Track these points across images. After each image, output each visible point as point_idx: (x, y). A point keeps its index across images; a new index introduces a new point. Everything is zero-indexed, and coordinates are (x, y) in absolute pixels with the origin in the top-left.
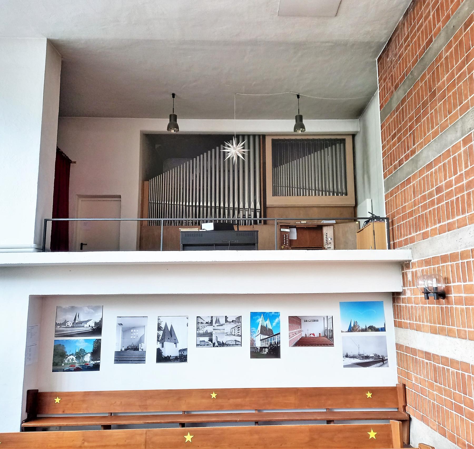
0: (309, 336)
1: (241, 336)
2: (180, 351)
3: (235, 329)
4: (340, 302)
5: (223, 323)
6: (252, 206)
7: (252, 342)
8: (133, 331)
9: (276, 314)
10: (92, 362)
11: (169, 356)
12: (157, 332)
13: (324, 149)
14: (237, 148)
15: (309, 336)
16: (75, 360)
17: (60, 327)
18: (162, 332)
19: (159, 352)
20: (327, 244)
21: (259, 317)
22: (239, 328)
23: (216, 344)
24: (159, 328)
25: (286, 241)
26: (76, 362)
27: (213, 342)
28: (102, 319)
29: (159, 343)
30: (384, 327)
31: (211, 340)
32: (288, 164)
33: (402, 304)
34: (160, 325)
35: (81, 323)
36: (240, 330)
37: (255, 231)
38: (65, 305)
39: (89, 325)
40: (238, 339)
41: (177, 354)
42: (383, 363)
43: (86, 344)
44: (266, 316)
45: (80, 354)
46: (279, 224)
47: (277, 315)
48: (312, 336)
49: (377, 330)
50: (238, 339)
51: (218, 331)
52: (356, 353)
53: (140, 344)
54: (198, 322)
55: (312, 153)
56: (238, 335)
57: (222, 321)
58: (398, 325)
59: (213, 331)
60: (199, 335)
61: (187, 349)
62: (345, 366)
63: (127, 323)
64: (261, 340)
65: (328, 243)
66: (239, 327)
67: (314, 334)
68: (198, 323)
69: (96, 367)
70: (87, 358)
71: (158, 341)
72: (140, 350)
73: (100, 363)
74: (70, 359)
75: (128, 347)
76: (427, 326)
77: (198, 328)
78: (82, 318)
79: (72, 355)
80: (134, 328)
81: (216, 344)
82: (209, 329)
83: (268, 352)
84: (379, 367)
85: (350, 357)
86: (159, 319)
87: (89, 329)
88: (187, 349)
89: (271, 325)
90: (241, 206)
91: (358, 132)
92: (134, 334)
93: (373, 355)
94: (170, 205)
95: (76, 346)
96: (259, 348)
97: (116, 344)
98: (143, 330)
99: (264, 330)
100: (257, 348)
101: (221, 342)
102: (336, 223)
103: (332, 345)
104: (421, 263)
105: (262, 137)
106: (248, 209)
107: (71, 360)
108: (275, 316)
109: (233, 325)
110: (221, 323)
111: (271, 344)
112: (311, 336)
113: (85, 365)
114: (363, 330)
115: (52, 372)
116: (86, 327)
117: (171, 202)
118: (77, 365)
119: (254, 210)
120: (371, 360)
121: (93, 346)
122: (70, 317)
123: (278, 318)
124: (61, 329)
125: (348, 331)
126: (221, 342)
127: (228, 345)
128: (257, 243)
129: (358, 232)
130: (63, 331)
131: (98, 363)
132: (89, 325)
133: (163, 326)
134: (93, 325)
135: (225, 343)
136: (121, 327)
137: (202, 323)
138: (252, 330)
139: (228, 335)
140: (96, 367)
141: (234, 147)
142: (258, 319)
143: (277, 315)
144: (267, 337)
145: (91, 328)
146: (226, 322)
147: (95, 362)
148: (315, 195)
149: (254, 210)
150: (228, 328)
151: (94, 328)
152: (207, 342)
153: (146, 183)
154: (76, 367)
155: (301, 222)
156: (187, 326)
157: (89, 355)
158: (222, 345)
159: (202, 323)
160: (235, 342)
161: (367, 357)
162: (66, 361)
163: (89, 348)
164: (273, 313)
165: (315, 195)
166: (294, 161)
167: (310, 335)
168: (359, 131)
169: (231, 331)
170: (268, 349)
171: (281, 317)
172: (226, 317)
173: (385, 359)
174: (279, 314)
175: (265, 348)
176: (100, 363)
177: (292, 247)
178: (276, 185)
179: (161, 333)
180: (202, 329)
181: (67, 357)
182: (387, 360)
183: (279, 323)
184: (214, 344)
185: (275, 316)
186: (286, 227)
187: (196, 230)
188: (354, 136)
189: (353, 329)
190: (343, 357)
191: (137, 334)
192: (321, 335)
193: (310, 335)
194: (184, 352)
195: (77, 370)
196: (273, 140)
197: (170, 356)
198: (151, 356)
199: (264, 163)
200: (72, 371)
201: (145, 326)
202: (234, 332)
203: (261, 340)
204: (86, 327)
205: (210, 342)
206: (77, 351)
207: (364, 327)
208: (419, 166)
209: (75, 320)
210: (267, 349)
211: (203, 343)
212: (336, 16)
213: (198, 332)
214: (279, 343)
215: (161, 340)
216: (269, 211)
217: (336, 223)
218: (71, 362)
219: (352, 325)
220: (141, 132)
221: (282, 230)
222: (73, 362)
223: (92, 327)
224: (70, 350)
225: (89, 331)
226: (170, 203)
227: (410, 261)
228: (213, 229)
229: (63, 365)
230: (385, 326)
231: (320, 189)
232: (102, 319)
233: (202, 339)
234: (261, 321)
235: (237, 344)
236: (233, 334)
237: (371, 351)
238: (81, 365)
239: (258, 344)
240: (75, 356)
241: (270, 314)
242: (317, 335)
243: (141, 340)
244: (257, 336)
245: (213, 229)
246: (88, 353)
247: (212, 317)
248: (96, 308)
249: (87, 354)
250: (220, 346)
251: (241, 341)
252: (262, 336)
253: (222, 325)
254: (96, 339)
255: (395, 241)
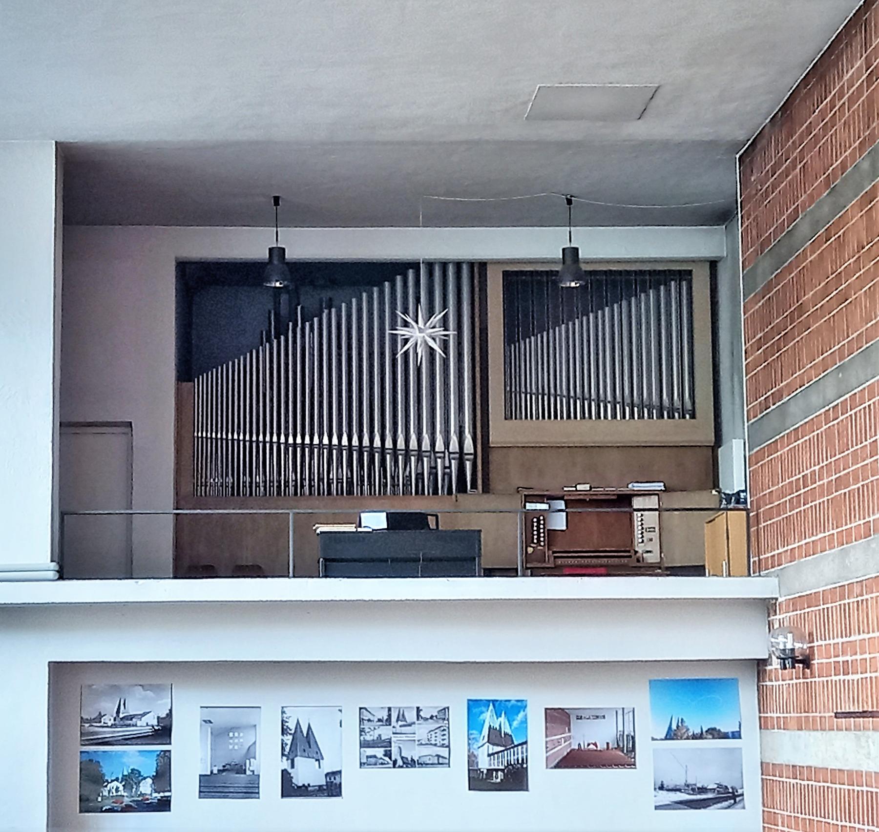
0: (586, 747)
1: (448, 746)
2: (327, 775)
3: (436, 733)
4: (650, 681)
5: (413, 721)
6: (454, 446)
7: (472, 759)
8: (239, 734)
9: (519, 704)
10: (155, 795)
11: (306, 785)
12: (281, 737)
13: (636, 296)
14: (426, 329)
15: (586, 747)
16: (123, 791)
17: (90, 726)
18: (291, 737)
19: (286, 776)
20: (643, 542)
21: (484, 709)
22: (445, 731)
23: (400, 762)
24: (284, 731)
25: (539, 537)
26: (125, 794)
27: (393, 759)
28: (171, 710)
29: (285, 758)
30: (738, 730)
31: (388, 754)
32: (545, 333)
33: (768, 683)
34: (287, 724)
35: (131, 717)
36: (447, 735)
37: (474, 531)
38: (100, 682)
39: (147, 724)
40: (444, 752)
41: (323, 782)
42: (735, 802)
43: (143, 759)
44: (499, 707)
45: (132, 779)
46: (521, 492)
47: (521, 705)
48: (592, 747)
49: (725, 736)
50: (444, 752)
51: (404, 737)
52: (681, 782)
53: (248, 762)
54: (363, 719)
55: (607, 306)
56: (443, 746)
57: (411, 716)
58: (764, 724)
59: (393, 736)
60: (364, 745)
61: (340, 772)
62: (657, 808)
63: (221, 718)
64: (489, 755)
65: (645, 540)
66: (445, 728)
67: (595, 744)
68: (361, 720)
69: (164, 805)
70: (146, 787)
71: (283, 755)
72: (248, 772)
73: (170, 796)
74: (113, 788)
75: (224, 766)
76: (794, 717)
77: (362, 731)
78: (132, 709)
79: (117, 780)
80: (233, 729)
81: (400, 762)
82: (385, 732)
83: (502, 778)
84: (726, 808)
85: (668, 790)
86: (283, 712)
87: (148, 730)
88: (340, 772)
89: (510, 725)
90: (426, 445)
91: (723, 257)
92: (236, 741)
93: (716, 786)
94: (254, 445)
95: (123, 764)
96: (485, 771)
97: (201, 759)
98: (252, 732)
99: (496, 737)
100: (482, 770)
101: (410, 759)
102: (667, 490)
103: (633, 765)
104: (795, 603)
105: (479, 268)
106: (444, 453)
107: (114, 791)
108: (518, 707)
109: (432, 724)
110: (409, 721)
111: (509, 764)
112: (590, 747)
113: (142, 800)
114: (695, 737)
115: (81, 812)
116: (141, 726)
117: (251, 436)
118: (127, 801)
119: (457, 456)
120: (710, 795)
121: (157, 764)
122: (109, 707)
123: (524, 711)
124: (92, 729)
125: (666, 739)
126: (410, 759)
127: (422, 765)
128: (480, 557)
129: (707, 523)
130: (97, 733)
131: (168, 797)
132: (147, 724)
133: (292, 725)
134: (155, 722)
135: (418, 761)
136: (208, 727)
137: (369, 720)
138: (471, 734)
139: (421, 744)
140: (164, 805)
141: (420, 329)
142: (482, 712)
143: (521, 705)
144: (503, 748)
145: (151, 728)
146: (418, 719)
147: (162, 794)
148: (614, 416)
149: (457, 456)
150: (422, 731)
151: (156, 728)
152: (381, 758)
153: (187, 385)
154: (124, 803)
155: (575, 487)
156: (341, 726)
157: (149, 781)
158: (410, 763)
159: (369, 720)
160: (436, 758)
161: (703, 790)
162: (106, 793)
163: (149, 768)
164: (513, 702)
165: (614, 416)
166: (560, 326)
167: (589, 745)
168: (725, 255)
169: (429, 737)
170: (504, 772)
171: (528, 709)
172: (418, 708)
173: (739, 793)
174: (525, 705)
175: (497, 770)
176: (170, 796)
177: (555, 550)
178: (513, 389)
179: (288, 739)
180: (370, 733)
181: (107, 785)
182: (742, 795)
183: (525, 721)
184: (395, 762)
185: (518, 707)
186: (540, 499)
187: (351, 528)
188: (713, 264)
189: (675, 734)
190: (655, 789)
191: (241, 740)
192: (611, 746)
193: (589, 745)
194: (335, 779)
195: (127, 809)
196: (506, 274)
197: (309, 785)
198: (271, 784)
199: (484, 331)
200: (117, 811)
201: (255, 726)
202: (433, 738)
203: (489, 755)
204: (141, 726)
205: (387, 759)
206: (126, 773)
207: (698, 731)
208: (787, 425)
209: (118, 712)
210: (502, 774)
211: (373, 760)
212: (639, 118)
213: (362, 738)
214: (525, 761)
215: (290, 754)
216: (494, 457)
217: (667, 490)
218: (115, 794)
219: (674, 727)
220: (176, 259)
221: (529, 506)
222: (119, 793)
223: (153, 727)
224: (112, 770)
225: (148, 734)
226: (247, 438)
227: (777, 599)
228: (386, 527)
229: (100, 799)
230: (740, 728)
231: (628, 400)
232: (171, 710)
233: (370, 751)
234: (489, 718)
235: (441, 762)
236: (433, 742)
237: (709, 778)
238: (134, 801)
239: (484, 764)
240: (123, 783)
241: (507, 703)
242: (601, 746)
243: (250, 753)
244: (482, 746)
245: (386, 527)
246: (147, 777)
247: (390, 709)
248: (156, 688)
249: (145, 778)
250: (407, 767)
251: (448, 757)
252: (491, 746)
253: (410, 725)
254: (162, 751)
255: (761, 557)
